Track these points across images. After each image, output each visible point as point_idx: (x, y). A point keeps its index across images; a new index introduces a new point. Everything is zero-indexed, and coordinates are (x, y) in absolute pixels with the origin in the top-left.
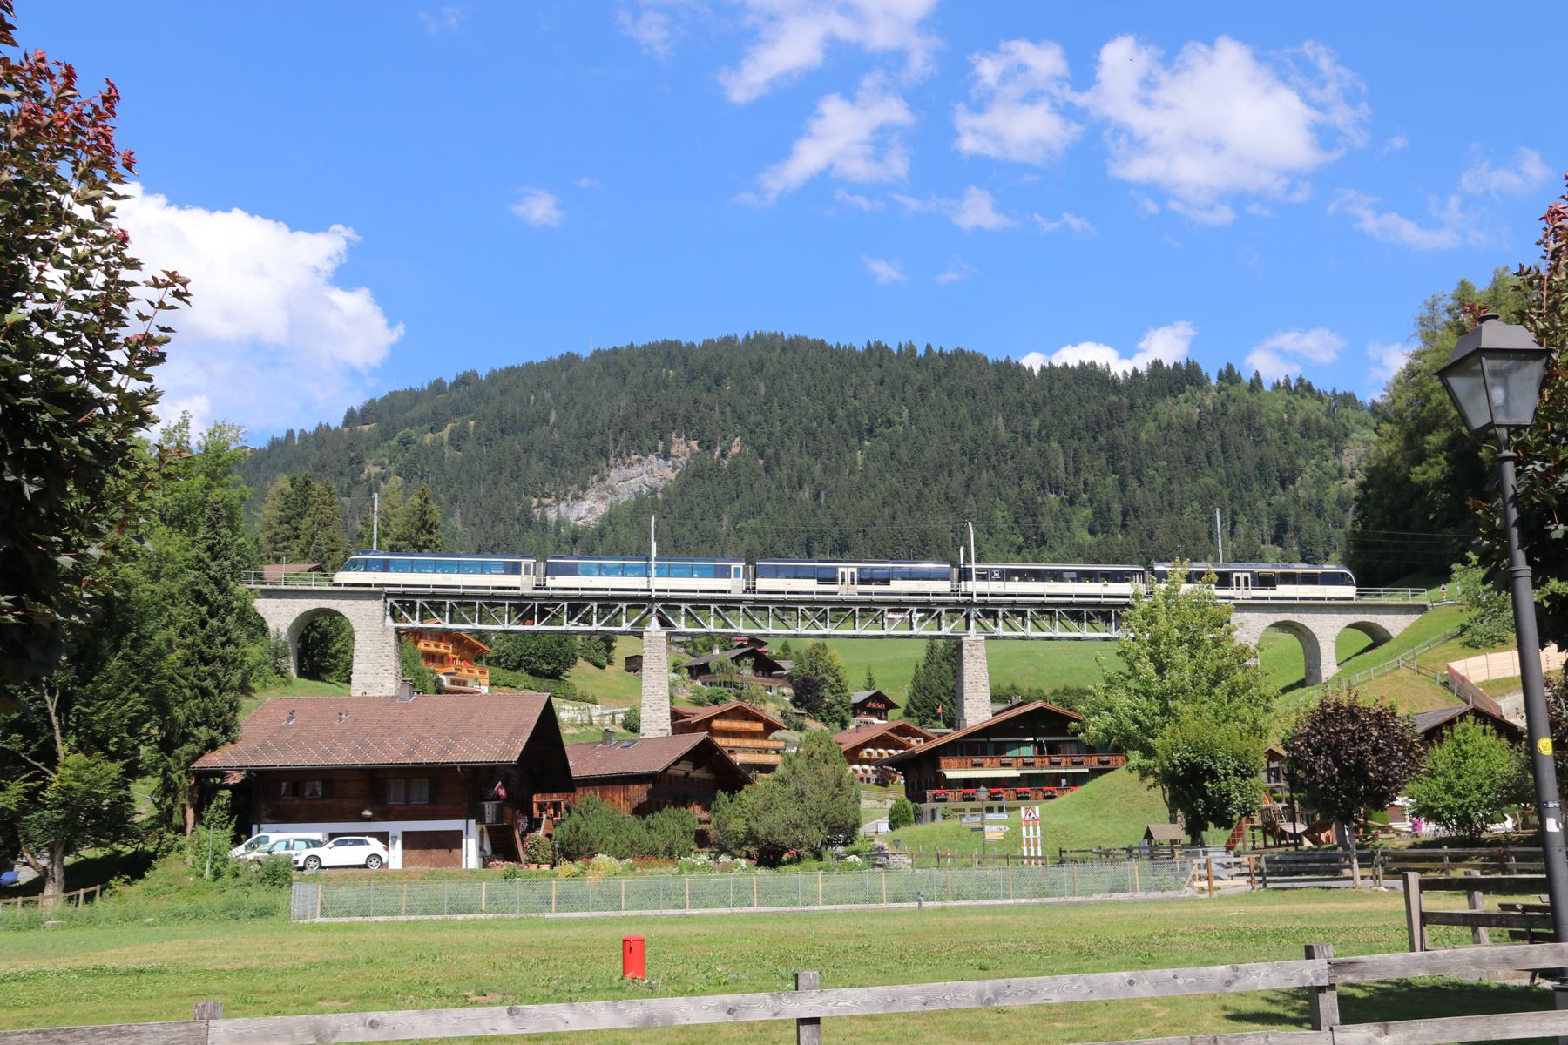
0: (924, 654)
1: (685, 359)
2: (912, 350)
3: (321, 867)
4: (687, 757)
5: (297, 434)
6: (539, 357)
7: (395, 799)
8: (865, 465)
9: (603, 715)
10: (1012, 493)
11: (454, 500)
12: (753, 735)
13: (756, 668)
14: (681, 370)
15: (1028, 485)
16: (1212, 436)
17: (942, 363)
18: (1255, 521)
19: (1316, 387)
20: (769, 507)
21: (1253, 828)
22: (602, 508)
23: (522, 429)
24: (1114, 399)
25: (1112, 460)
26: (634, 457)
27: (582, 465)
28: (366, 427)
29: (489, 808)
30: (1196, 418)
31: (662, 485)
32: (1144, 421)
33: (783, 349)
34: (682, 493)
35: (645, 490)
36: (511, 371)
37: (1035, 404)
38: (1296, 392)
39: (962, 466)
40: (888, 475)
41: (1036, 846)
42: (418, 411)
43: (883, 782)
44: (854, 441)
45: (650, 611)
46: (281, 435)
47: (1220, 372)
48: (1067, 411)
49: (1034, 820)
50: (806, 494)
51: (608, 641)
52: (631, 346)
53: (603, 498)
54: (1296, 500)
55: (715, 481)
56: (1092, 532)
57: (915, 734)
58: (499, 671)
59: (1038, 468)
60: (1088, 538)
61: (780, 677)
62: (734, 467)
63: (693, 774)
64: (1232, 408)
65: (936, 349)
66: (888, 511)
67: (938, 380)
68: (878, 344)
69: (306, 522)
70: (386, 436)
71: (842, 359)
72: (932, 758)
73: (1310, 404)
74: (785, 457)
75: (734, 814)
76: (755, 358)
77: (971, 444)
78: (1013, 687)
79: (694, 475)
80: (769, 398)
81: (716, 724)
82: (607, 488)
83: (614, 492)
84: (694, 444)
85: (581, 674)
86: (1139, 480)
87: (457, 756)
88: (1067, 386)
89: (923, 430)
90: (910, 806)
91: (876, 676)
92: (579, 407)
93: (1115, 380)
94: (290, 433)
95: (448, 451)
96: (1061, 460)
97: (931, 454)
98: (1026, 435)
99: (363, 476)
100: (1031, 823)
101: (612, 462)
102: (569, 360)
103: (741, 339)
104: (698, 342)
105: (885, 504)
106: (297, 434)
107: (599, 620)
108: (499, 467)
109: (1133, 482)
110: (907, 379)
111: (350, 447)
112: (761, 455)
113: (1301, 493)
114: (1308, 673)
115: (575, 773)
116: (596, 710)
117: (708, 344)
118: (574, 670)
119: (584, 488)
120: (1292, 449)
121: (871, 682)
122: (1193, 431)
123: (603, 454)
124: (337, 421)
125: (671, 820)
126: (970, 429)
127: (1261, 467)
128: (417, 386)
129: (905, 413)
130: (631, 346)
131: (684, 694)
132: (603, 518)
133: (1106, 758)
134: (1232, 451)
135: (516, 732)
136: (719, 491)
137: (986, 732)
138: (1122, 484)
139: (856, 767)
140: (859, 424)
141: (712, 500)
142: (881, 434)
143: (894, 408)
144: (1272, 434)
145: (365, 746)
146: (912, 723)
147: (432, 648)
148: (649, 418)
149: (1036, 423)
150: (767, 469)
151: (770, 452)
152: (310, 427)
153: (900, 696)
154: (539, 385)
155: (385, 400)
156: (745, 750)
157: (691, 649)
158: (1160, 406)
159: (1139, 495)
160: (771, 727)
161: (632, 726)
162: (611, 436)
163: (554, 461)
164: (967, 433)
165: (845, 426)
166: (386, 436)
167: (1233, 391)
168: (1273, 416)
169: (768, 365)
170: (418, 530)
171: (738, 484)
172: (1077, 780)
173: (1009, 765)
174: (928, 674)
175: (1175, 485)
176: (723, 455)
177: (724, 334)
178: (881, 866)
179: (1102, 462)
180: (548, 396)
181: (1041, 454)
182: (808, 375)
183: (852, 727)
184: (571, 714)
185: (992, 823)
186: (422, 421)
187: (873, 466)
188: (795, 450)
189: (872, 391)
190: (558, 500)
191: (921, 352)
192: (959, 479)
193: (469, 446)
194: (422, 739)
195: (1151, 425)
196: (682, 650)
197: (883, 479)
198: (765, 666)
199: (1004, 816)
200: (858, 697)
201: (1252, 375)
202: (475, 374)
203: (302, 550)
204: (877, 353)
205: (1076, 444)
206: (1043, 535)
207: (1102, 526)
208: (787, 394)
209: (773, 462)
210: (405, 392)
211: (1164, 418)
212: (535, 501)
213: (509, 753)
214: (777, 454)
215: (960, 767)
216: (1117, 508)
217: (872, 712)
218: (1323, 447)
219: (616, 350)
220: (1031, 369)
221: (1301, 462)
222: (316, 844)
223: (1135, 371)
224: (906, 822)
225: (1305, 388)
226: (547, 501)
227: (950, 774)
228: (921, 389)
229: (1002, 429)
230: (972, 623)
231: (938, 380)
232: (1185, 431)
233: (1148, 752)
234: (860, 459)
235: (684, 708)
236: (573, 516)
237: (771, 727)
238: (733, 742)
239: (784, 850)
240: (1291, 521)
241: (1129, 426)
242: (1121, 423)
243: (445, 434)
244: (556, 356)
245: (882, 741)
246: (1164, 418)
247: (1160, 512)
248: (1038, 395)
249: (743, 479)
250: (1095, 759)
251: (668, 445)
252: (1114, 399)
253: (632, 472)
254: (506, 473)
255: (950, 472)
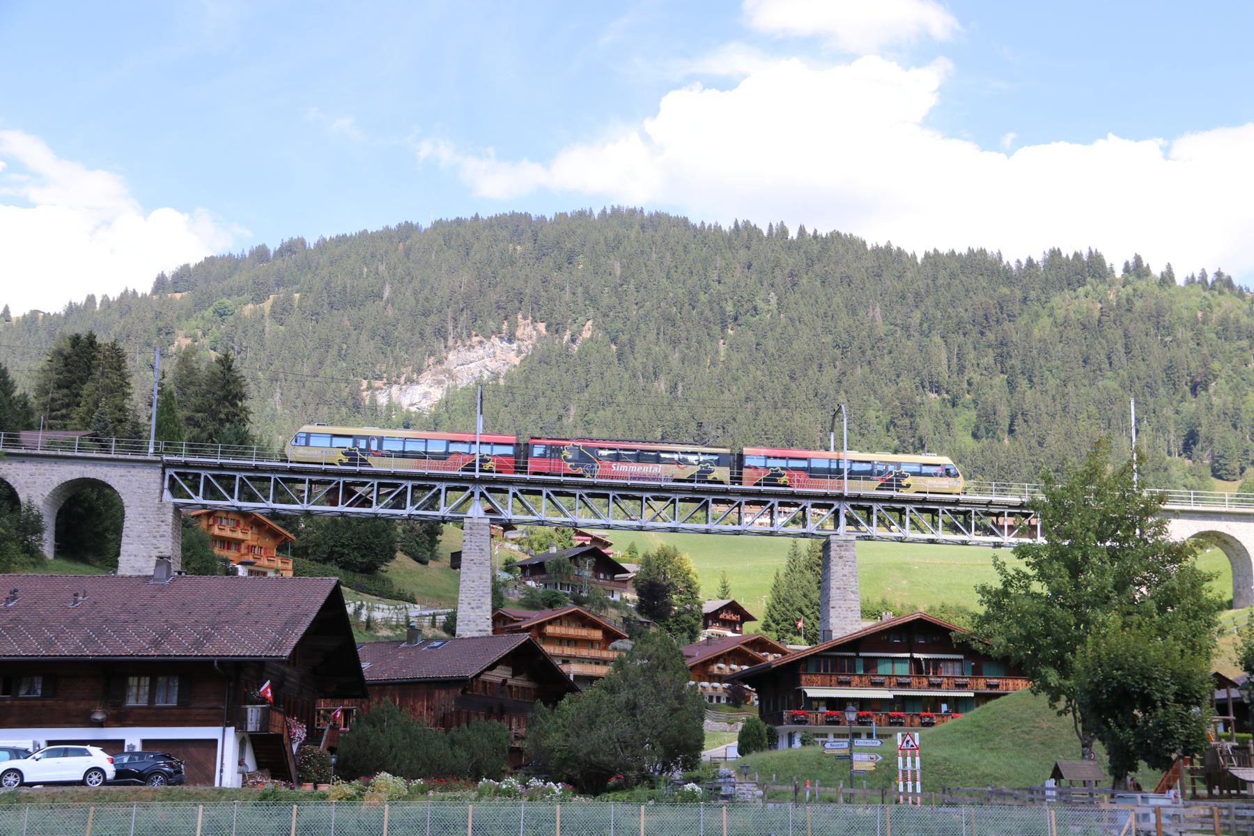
0: (785, 562)
1: (535, 234)
2: (783, 231)
3: (22, 784)
4: (504, 661)
5: (98, 300)
6: (374, 226)
7: (137, 696)
8: (728, 355)
9: (421, 616)
10: (888, 391)
11: (274, 379)
12: (590, 643)
13: (596, 570)
14: (529, 245)
15: (906, 383)
16: (1116, 334)
17: (816, 248)
18: (1160, 429)
19: (1236, 282)
20: (621, 399)
21: (1192, 772)
22: (438, 394)
23: (353, 304)
24: (1005, 290)
25: (1001, 358)
26: (475, 339)
27: (418, 345)
28: (178, 296)
29: (253, 715)
30: (1097, 314)
31: (504, 370)
32: (1037, 315)
33: (643, 227)
34: (527, 379)
35: (486, 375)
36: (341, 240)
37: (917, 294)
38: (1213, 288)
39: (835, 359)
40: (751, 367)
41: (914, 781)
42: (237, 279)
43: (737, 699)
44: (716, 329)
45: (472, 494)
46: (80, 300)
47: (1127, 264)
48: (952, 303)
49: (913, 748)
50: (662, 385)
51: (432, 530)
52: (476, 218)
53: (440, 383)
54: (1210, 407)
55: (563, 367)
56: (975, 436)
57: (773, 649)
58: (304, 562)
59: (918, 365)
60: (969, 440)
61: (625, 581)
62: (584, 352)
63: (510, 682)
64: (1138, 304)
65: (810, 231)
66: (750, 405)
67: (811, 264)
68: (747, 223)
69: (87, 388)
70: (199, 305)
71: (708, 238)
72: (794, 670)
73: (1227, 302)
74: (640, 344)
75: (555, 728)
76: (611, 235)
77: (844, 336)
78: (884, 602)
79: (540, 360)
80: (625, 280)
81: (550, 630)
82: (444, 372)
83: (452, 376)
84: (542, 327)
85: (400, 567)
86: (1031, 381)
87: (210, 650)
88: (953, 276)
89: (792, 320)
90: (764, 727)
91: (732, 583)
92: (416, 283)
93: (1007, 270)
94: (91, 299)
95: (269, 325)
96: (944, 356)
97: (800, 346)
98: (906, 328)
99: (173, 349)
100: (909, 748)
101: (450, 342)
102: (408, 230)
103: (596, 212)
104: (550, 216)
105: (748, 399)
106: (98, 300)
107: (413, 503)
108: (326, 344)
109: (1023, 383)
110: (777, 264)
111: (158, 315)
112: (614, 340)
113: (1216, 401)
114: (1237, 593)
115: (368, 677)
116: (414, 611)
117: (561, 217)
118: (392, 565)
119: (420, 371)
120: (1205, 350)
121: (725, 589)
122: (1092, 328)
123: (441, 333)
124: (145, 287)
125: (482, 733)
126: (844, 320)
127: (1169, 369)
128: (236, 252)
129: (773, 298)
130: (476, 218)
131: (514, 595)
132: (438, 405)
133: (995, 681)
134: (1136, 352)
135: (293, 622)
136: (567, 379)
137: (856, 644)
138: (1011, 384)
139: (705, 684)
140: (723, 312)
141: (558, 388)
142: (746, 322)
143: (762, 294)
144: (1182, 333)
145: (100, 633)
146: (772, 637)
147: (227, 533)
148: (493, 296)
149: (917, 316)
150: (620, 356)
151: (624, 338)
152: (114, 295)
153: (758, 606)
154: (373, 256)
155: (199, 266)
156: (581, 660)
157: (526, 547)
158: (1056, 300)
159: (1029, 396)
160: (610, 636)
161: (450, 626)
162: (450, 314)
163: (387, 340)
164: (840, 323)
165: (707, 312)
166: (199, 305)
167: (1141, 285)
168: (1185, 314)
169: (625, 243)
170: (219, 401)
171: (588, 372)
172: (957, 705)
173: (881, 685)
174: (790, 587)
175: (1070, 388)
176: (573, 341)
177: (578, 209)
178: (725, 797)
179: (988, 360)
180: (382, 268)
181: (922, 348)
182: (668, 255)
183: (702, 639)
184: (386, 614)
185: (862, 750)
186: (240, 292)
187: (735, 356)
188: (652, 336)
189: (738, 273)
190: (390, 383)
191: (793, 234)
192: (831, 374)
193: (293, 320)
194: (174, 627)
195: (1046, 321)
196: (516, 547)
197: (747, 372)
198: (610, 567)
199: (876, 743)
200: (709, 607)
201: (1164, 269)
202: (302, 242)
203: (83, 419)
204: (745, 234)
205: (961, 339)
206: (921, 440)
207: (988, 431)
208: (645, 276)
209: (627, 349)
210: (223, 258)
211: (1061, 313)
212: (365, 383)
213: (280, 646)
214: (631, 341)
215: (823, 685)
216: (1004, 412)
217: (726, 624)
218: (1242, 349)
219: (459, 221)
220: (914, 256)
221: (1216, 365)
222: (25, 754)
223: (1030, 261)
224: (759, 747)
225: (1224, 283)
226: (378, 384)
227: (812, 692)
228: (791, 275)
229: (879, 321)
230: (843, 520)
231: (811, 264)
232: (1084, 327)
233: (1064, 669)
234: (722, 348)
235: (509, 610)
236: (405, 402)
237: (610, 636)
238: (568, 651)
239: (611, 774)
240: (1203, 431)
241: (1022, 321)
242: (1012, 318)
243: (267, 306)
244: (393, 226)
245: (735, 655)
246: (1061, 313)
247: (1053, 416)
248: (921, 285)
249: (593, 368)
250: (982, 682)
251: (514, 326)
252: (1005, 290)
253: (472, 355)
254: (333, 352)
255: (821, 366)
